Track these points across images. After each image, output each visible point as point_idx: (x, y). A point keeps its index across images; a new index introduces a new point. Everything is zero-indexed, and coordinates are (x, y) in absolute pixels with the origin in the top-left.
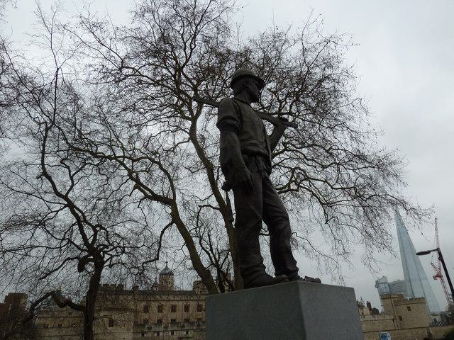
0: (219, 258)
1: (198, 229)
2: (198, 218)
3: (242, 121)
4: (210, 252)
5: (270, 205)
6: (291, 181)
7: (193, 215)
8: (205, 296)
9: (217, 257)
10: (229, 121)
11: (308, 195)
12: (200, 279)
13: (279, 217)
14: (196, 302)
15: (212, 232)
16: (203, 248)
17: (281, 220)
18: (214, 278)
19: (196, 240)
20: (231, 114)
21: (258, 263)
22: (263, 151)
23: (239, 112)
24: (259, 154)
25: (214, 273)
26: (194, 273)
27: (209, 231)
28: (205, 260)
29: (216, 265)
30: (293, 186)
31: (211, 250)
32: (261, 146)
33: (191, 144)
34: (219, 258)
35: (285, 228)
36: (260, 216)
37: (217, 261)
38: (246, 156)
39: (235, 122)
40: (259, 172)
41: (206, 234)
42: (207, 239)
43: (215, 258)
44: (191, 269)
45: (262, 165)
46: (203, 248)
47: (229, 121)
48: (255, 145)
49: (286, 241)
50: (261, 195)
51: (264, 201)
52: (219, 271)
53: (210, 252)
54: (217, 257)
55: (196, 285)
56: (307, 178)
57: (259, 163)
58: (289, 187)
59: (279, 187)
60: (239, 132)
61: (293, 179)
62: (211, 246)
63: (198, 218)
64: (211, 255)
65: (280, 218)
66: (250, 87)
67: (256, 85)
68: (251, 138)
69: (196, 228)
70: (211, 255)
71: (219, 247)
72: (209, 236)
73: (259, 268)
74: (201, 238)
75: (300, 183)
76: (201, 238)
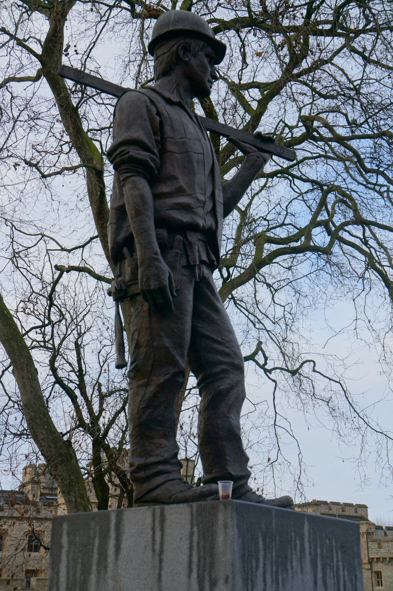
0: (101, 410)
1: (48, 329)
2: (50, 298)
3: (163, 151)
4: (77, 392)
5: (204, 336)
6: (314, 223)
7: (37, 287)
8: (156, 453)
9: (96, 408)
10: (135, 152)
11: (359, 264)
12: (42, 461)
13: (221, 363)
14: (26, 527)
15: (87, 338)
16: (59, 381)
17: (224, 371)
18: (83, 464)
19: (40, 357)
20: (138, 134)
21: (167, 455)
22: (201, 223)
23: (159, 128)
24: (193, 227)
25: (83, 448)
26: (27, 447)
27: (80, 335)
28: (61, 413)
29: (92, 428)
30: (320, 237)
31: (82, 386)
32: (200, 211)
33: (44, 88)
34: (101, 410)
35: (232, 388)
36: (183, 363)
37: (95, 419)
38: (164, 232)
39: (143, 155)
40: (190, 267)
41: (70, 343)
42: (72, 356)
43: (90, 411)
44: (19, 435)
45: (200, 252)
46: (59, 381)
47: (135, 152)
48: (187, 208)
49: (233, 416)
50: (189, 319)
51: (194, 330)
52: (99, 443)
53: (77, 392)
54: (96, 408)
55: (34, 475)
56: (359, 221)
57: (191, 247)
58: (309, 237)
59: (282, 233)
60: (154, 176)
61: (324, 216)
62: (81, 374)
63: (50, 298)
64: (80, 400)
65: (224, 367)
66: (193, 62)
67: (207, 56)
68: (180, 191)
69: (44, 326)
70: (80, 400)
71: (102, 380)
72: (78, 347)
73: (168, 467)
74: (55, 353)
75: (342, 227)
76: (55, 353)
